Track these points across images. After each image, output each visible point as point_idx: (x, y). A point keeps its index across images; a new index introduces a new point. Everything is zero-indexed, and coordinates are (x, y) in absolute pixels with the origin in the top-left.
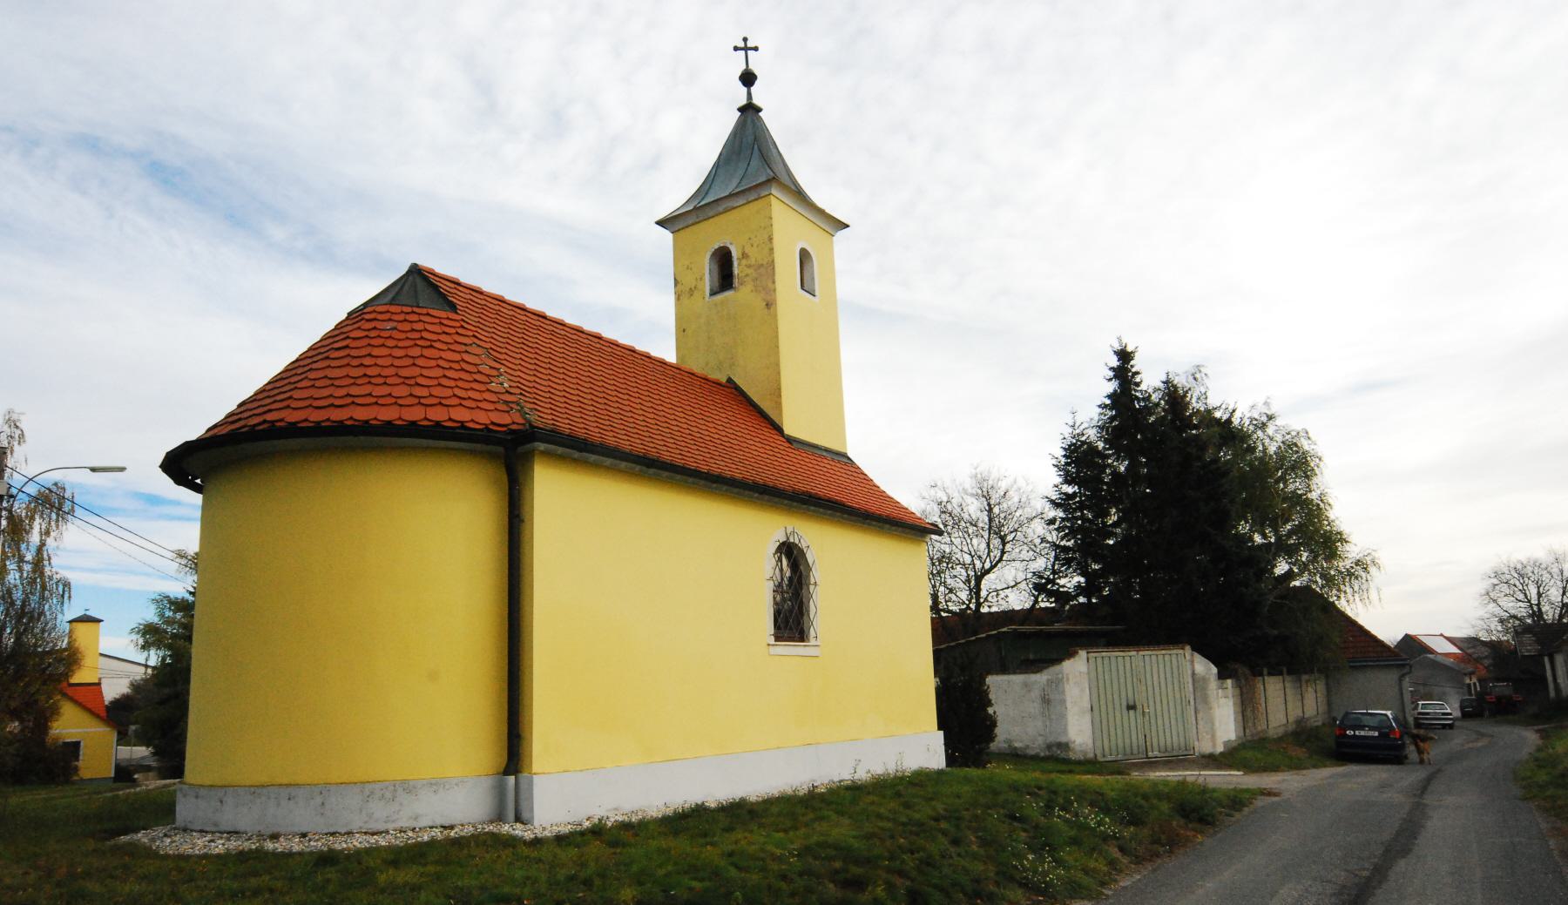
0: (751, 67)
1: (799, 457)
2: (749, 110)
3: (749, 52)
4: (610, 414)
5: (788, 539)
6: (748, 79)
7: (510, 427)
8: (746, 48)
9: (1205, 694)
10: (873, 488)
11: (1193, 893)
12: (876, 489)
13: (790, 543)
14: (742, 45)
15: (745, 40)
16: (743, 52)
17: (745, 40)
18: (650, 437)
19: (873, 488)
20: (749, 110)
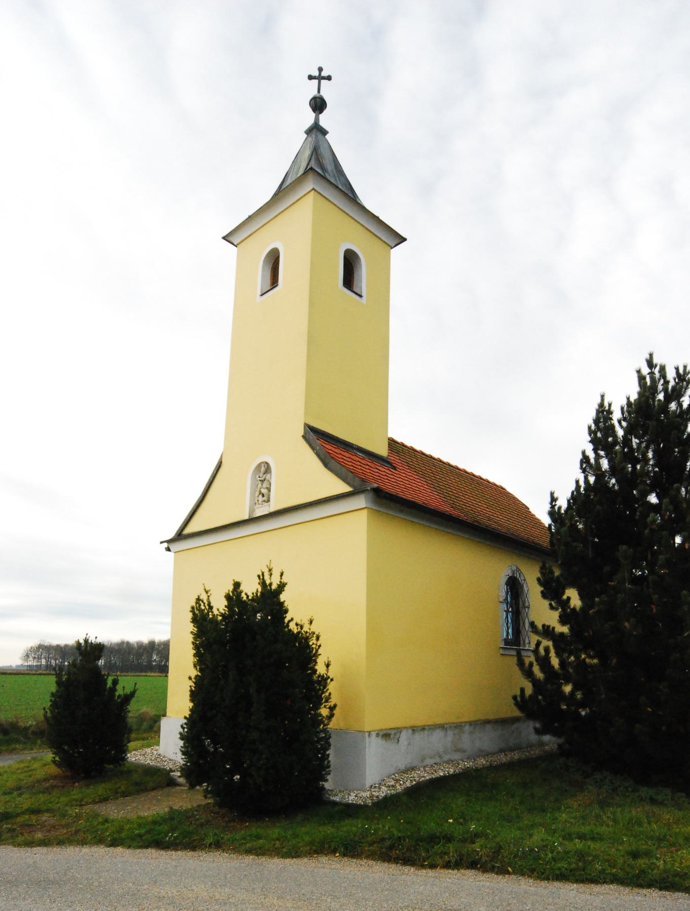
0: (322, 93)
1: (480, 504)
2: (316, 130)
3: (323, 81)
4: (389, 478)
5: (514, 574)
6: (318, 105)
7: (527, 619)
8: (320, 77)
9: (334, 852)
10: (517, 502)
11: (16, 745)
12: (537, 521)
13: (514, 577)
14: (316, 74)
15: (320, 69)
16: (317, 81)
17: (320, 69)
18: (395, 482)
19: (517, 502)
20: (316, 130)
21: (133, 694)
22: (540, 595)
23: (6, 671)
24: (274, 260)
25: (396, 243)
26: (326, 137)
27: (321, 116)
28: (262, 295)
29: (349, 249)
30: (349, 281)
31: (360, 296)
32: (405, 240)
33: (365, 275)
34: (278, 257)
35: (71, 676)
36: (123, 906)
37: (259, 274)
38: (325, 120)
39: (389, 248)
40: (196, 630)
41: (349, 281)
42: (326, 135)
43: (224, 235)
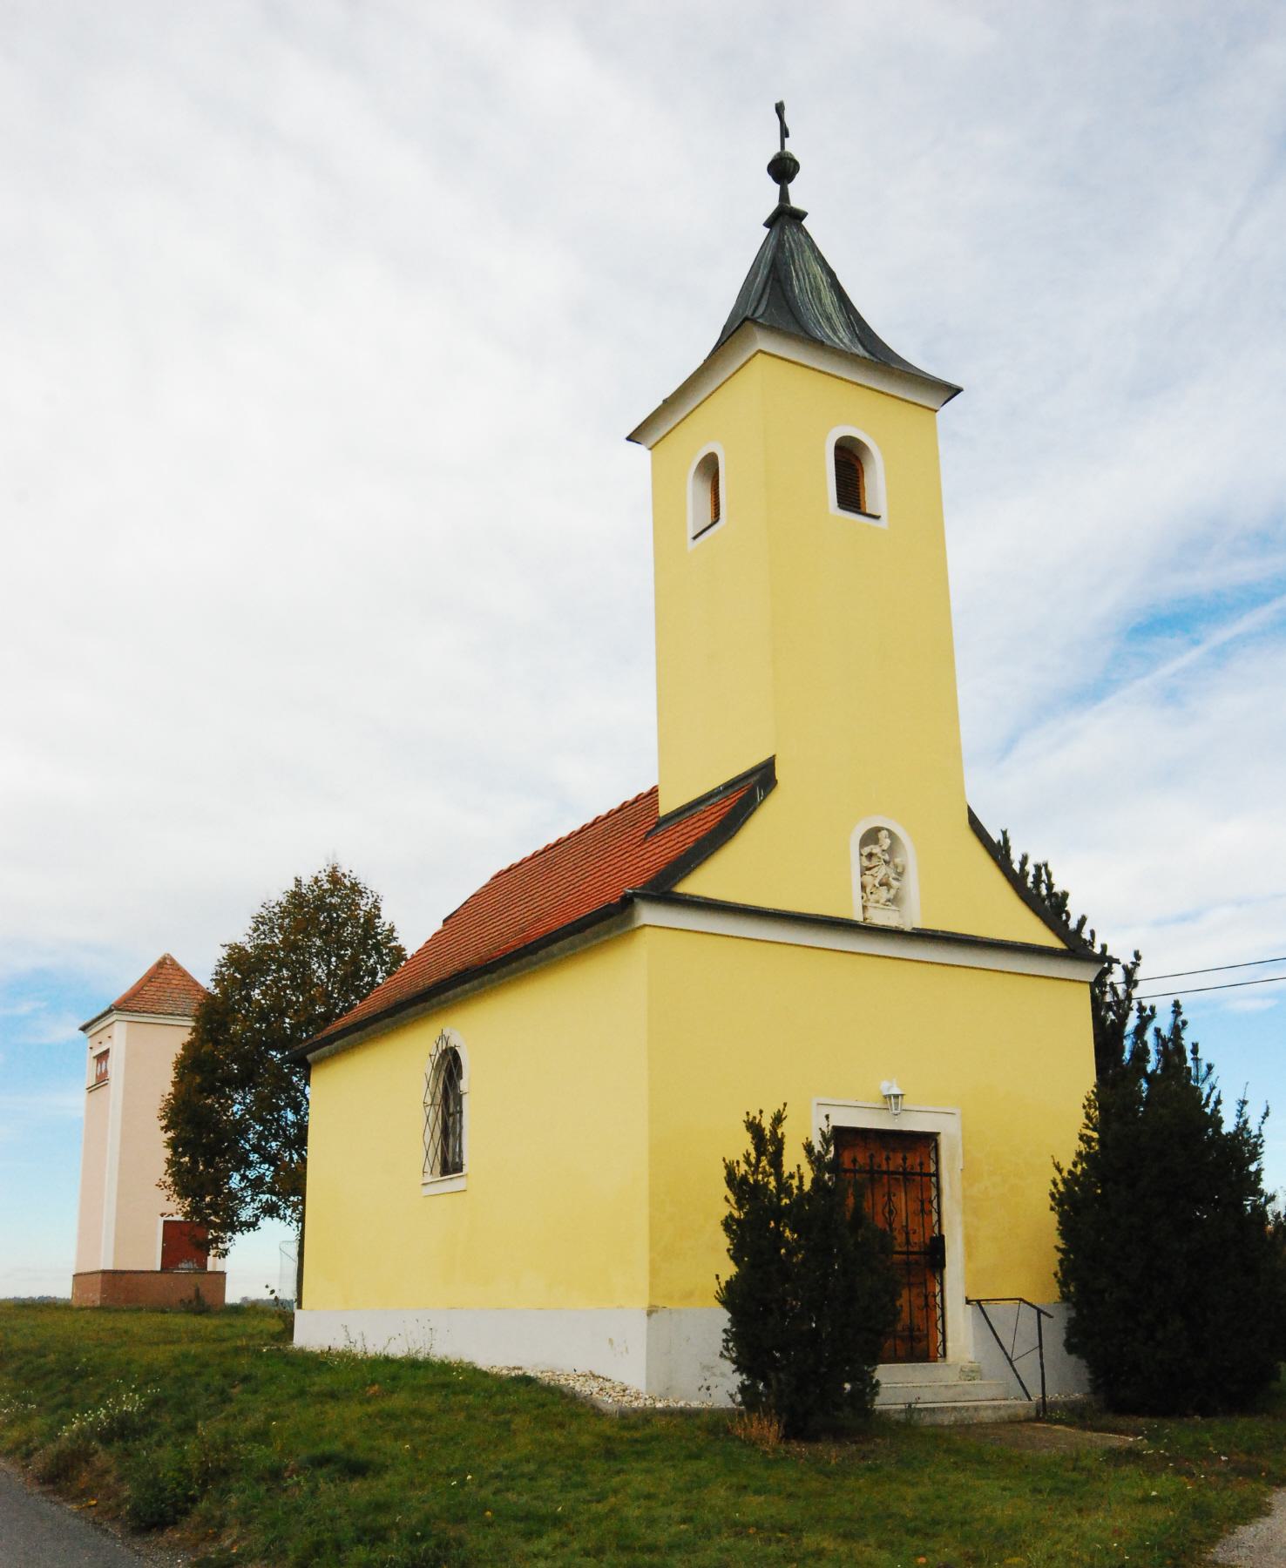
2: (786, 218)
6: (783, 169)
20: (786, 218)
21: (197, 1290)
22: (722, 1228)
23: (362, 1033)
24: (710, 468)
25: (948, 397)
26: (803, 223)
27: (790, 186)
28: (695, 538)
29: (844, 437)
30: (850, 494)
31: (877, 517)
32: (958, 391)
33: (877, 483)
34: (717, 464)
35: (1000, 1507)
36: (230, 1240)
37: (693, 494)
38: (799, 195)
39: (933, 413)
40: (807, 1186)
41: (850, 494)
42: (802, 219)
43: (627, 435)
